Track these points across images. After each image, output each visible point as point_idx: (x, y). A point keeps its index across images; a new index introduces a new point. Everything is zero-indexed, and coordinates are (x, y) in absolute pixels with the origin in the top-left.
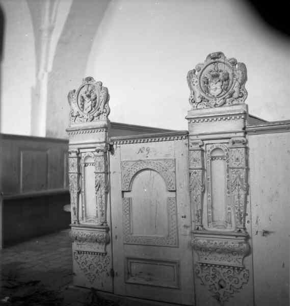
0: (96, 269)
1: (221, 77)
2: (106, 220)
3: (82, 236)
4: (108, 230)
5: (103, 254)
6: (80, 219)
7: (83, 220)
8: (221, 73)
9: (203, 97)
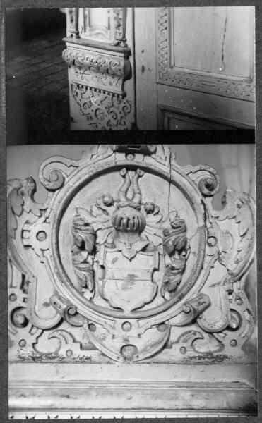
0: (106, 119)
1: (153, 234)
2: (124, 37)
3: (83, 60)
4: (127, 54)
5: (118, 96)
6: (80, 30)
7: (85, 31)
8: (151, 219)
9: (70, 307)
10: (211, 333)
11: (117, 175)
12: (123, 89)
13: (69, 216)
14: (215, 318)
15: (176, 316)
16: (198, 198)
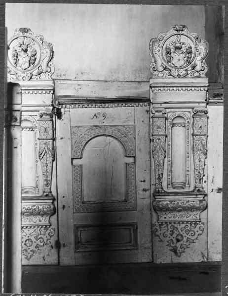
1: (184, 49)
8: (183, 46)
10: (197, 71)
11: (175, 36)
12: (49, 223)
13: (165, 46)
14: (198, 68)
15: (189, 68)
16: (194, 40)
